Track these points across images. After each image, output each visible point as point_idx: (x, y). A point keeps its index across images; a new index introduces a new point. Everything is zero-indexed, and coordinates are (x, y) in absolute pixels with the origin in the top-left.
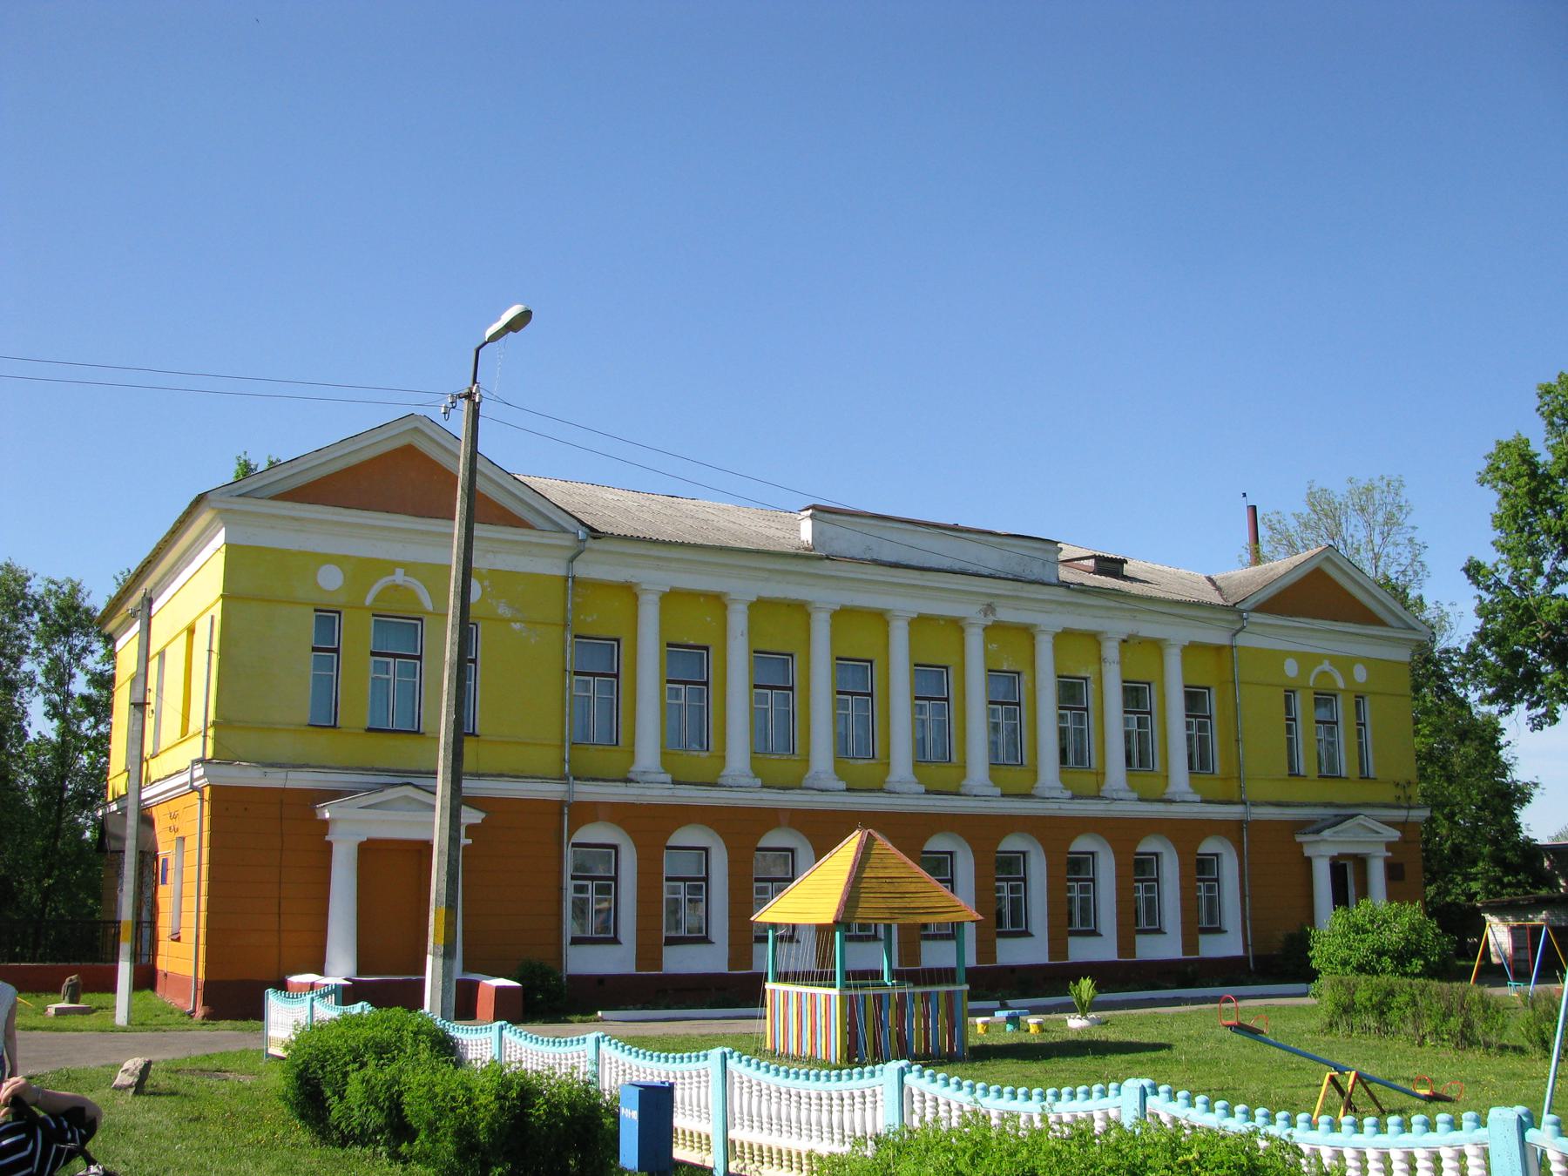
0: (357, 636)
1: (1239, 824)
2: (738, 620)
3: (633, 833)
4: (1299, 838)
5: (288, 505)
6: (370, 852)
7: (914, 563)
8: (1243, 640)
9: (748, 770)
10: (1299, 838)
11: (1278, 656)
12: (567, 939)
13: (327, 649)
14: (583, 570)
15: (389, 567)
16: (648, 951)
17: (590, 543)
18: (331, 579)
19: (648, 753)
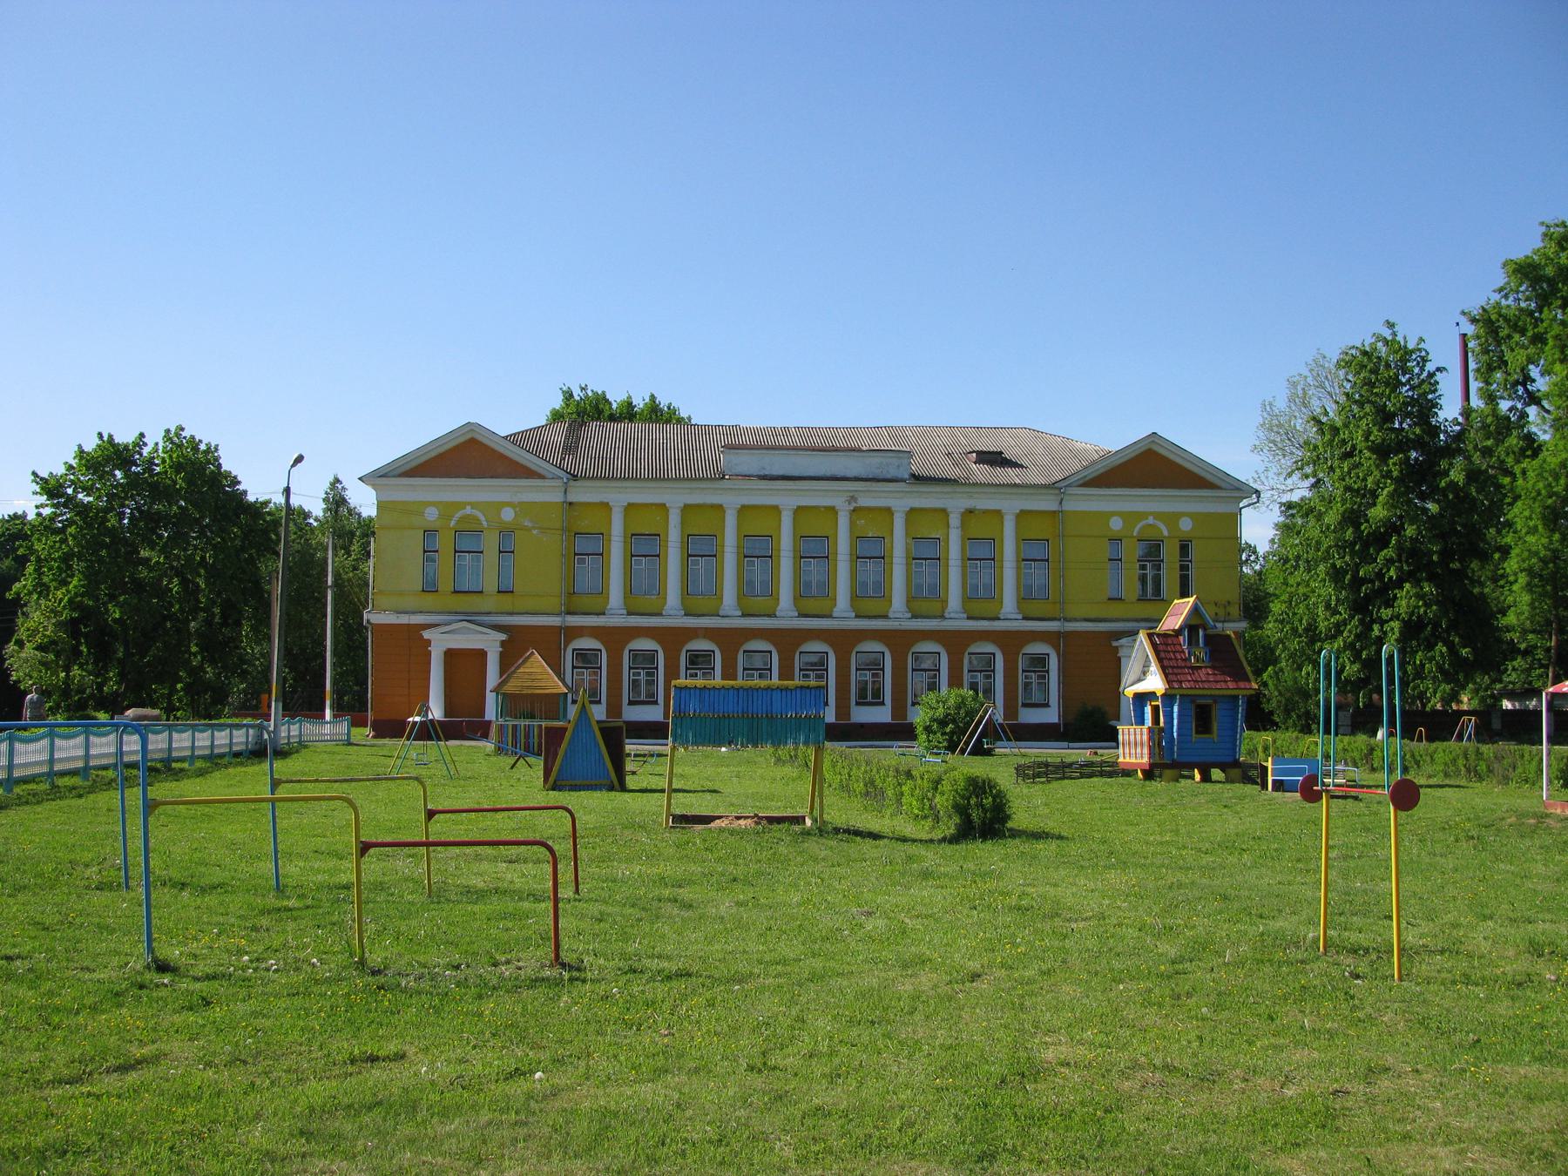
0: (445, 543)
1: (1058, 634)
2: (674, 519)
3: (832, 645)
4: (1115, 644)
5: (533, 467)
6: (450, 655)
7: (850, 474)
8: (1069, 506)
9: (904, 608)
10: (1115, 644)
11: (1106, 516)
12: (625, 700)
13: (429, 552)
14: (572, 498)
15: (463, 505)
16: (1010, 709)
17: (572, 483)
18: (432, 514)
19: (954, 601)
